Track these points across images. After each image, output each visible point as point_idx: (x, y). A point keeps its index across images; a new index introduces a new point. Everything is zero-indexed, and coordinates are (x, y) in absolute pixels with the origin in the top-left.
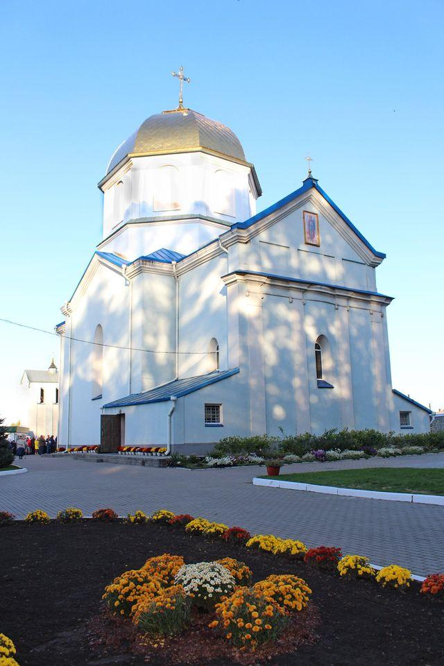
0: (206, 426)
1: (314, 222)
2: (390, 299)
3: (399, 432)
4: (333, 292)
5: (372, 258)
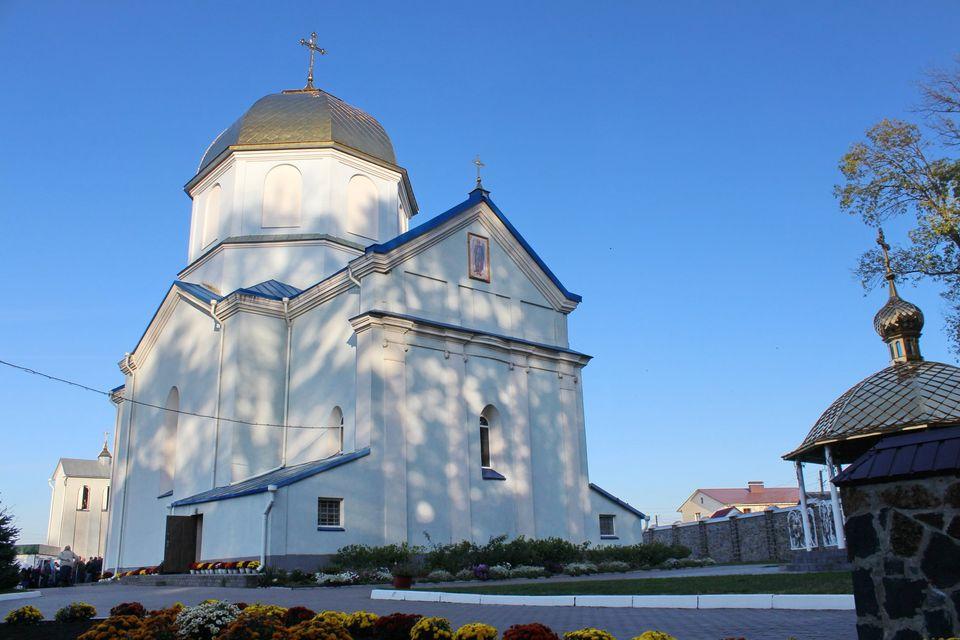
0: (320, 530)
1: (482, 248)
2: (588, 358)
3: (596, 543)
4: (507, 346)
5: (562, 301)
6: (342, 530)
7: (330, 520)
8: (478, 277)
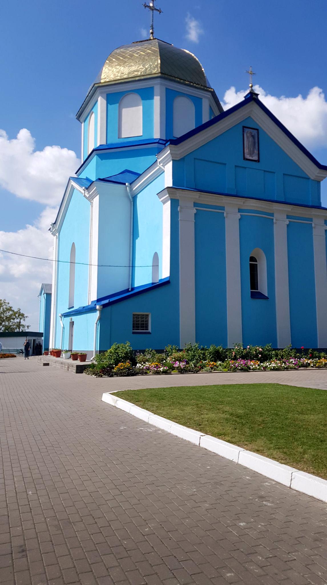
0: (134, 333)
6: (149, 333)
7: (141, 327)
8: (251, 158)
